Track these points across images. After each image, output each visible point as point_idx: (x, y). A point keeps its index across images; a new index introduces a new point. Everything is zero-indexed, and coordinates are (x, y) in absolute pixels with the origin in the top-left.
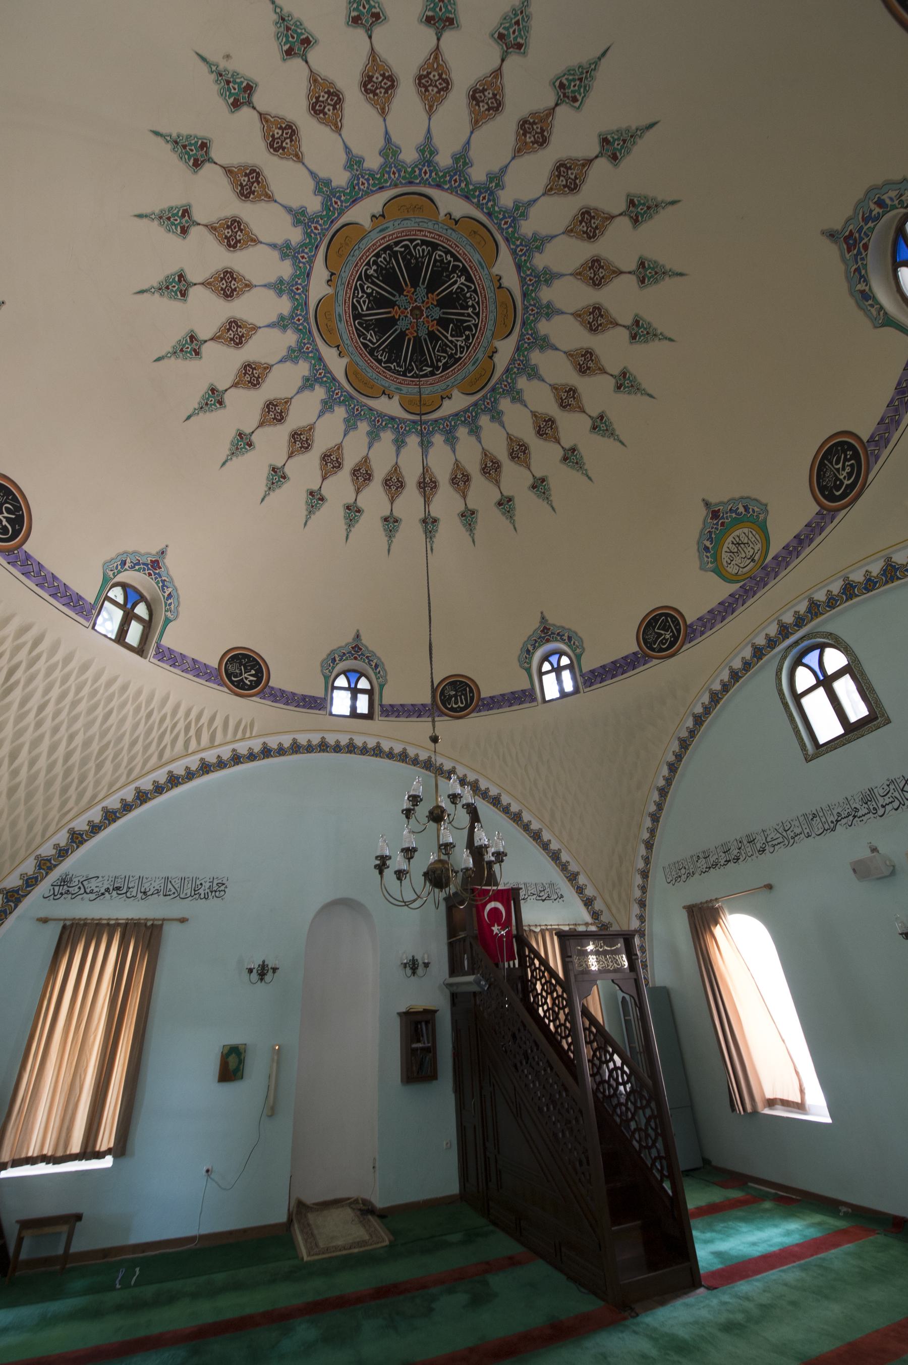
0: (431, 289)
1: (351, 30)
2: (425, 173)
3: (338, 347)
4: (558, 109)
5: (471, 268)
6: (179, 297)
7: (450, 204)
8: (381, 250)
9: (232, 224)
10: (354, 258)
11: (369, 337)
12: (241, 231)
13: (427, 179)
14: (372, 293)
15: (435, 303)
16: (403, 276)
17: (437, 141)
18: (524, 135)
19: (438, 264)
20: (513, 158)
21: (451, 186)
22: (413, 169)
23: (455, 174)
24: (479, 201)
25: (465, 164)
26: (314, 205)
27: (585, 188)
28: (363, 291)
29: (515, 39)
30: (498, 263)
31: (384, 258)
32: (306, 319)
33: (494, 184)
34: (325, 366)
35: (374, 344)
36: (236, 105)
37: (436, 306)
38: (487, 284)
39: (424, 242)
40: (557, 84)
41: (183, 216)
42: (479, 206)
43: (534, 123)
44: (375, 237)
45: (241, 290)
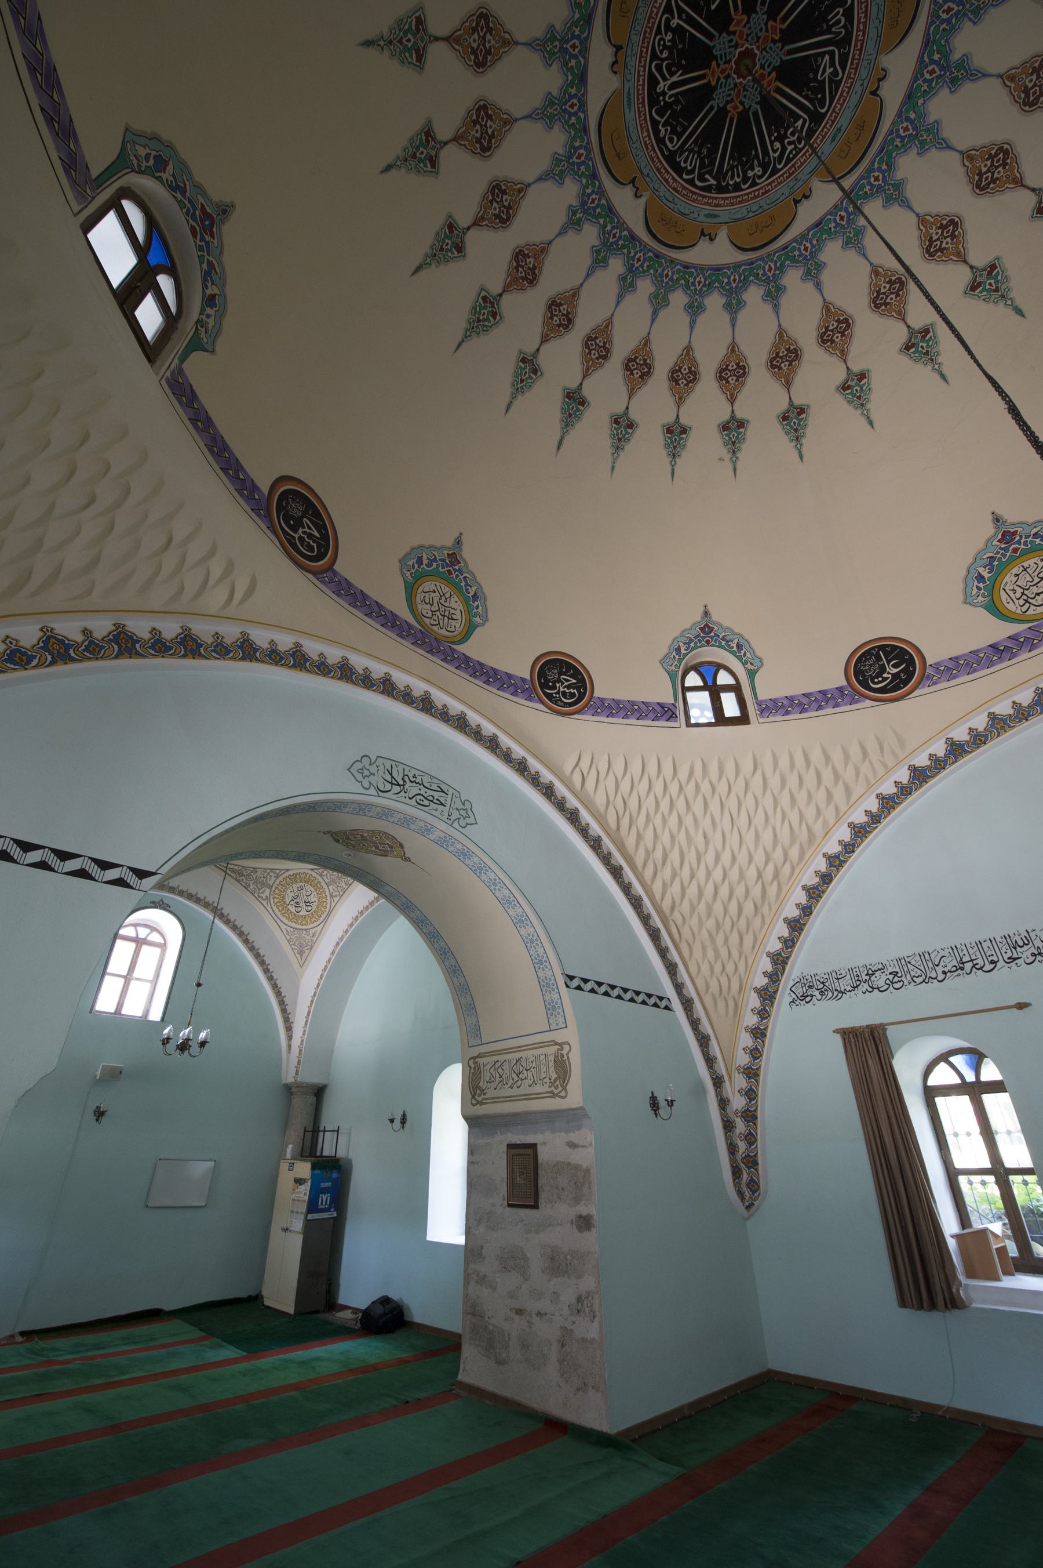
0: (706, 92)
1: (637, 421)
2: (639, 260)
3: (874, 93)
4: (500, 291)
5: (643, 103)
6: (931, 334)
7: (630, 207)
8: (729, 192)
9: (828, 341)
10: (762, 203)
11: (829, 71)
12: (827, 328)
13: (640, 251)
14: (776, 139)
15: (714, 63)
16: (728, 136)
17: (615, 290)
18: (535, 267)
19: (679, 129)
20: (551, 242)
21: (621, 232)
22: (648, 271)
23: (612, 243)
24: (600, 200)
25: (598, 252)
26: (753, 294)
27: (482, 187)
28: (784, 149)
29: (525, 368)
30: (608, 95)
31: (732, 178)
32: (870, 170)
33: (578, 215)
34: (915, 79)
35: (832, 54)
36: (742, 424)
37: (715, 58)
38: (633, 62)
39: (679, 171)
40: (498, 318)
41: (849, 387)
42: (601, 192)
43: (523, 279)
44: (725, 213)
45: (885, 276)
